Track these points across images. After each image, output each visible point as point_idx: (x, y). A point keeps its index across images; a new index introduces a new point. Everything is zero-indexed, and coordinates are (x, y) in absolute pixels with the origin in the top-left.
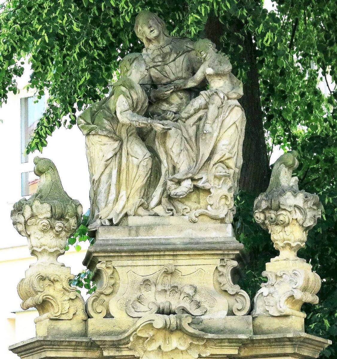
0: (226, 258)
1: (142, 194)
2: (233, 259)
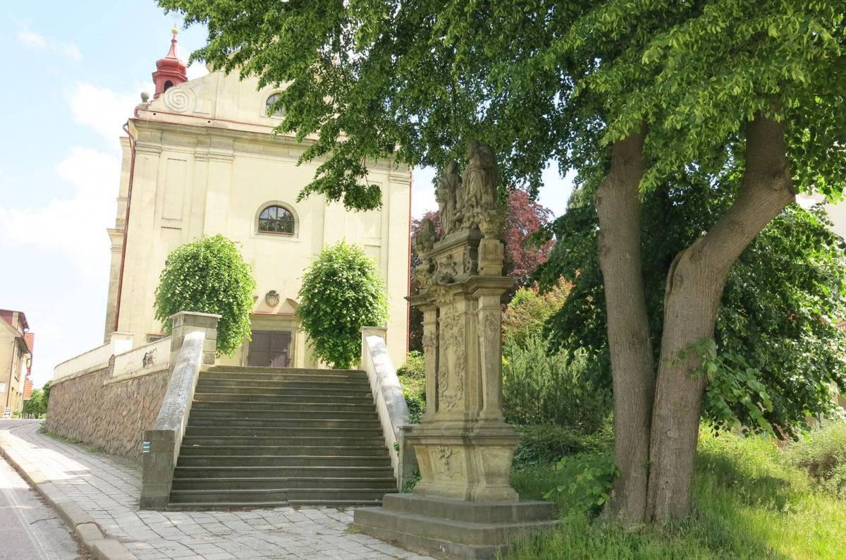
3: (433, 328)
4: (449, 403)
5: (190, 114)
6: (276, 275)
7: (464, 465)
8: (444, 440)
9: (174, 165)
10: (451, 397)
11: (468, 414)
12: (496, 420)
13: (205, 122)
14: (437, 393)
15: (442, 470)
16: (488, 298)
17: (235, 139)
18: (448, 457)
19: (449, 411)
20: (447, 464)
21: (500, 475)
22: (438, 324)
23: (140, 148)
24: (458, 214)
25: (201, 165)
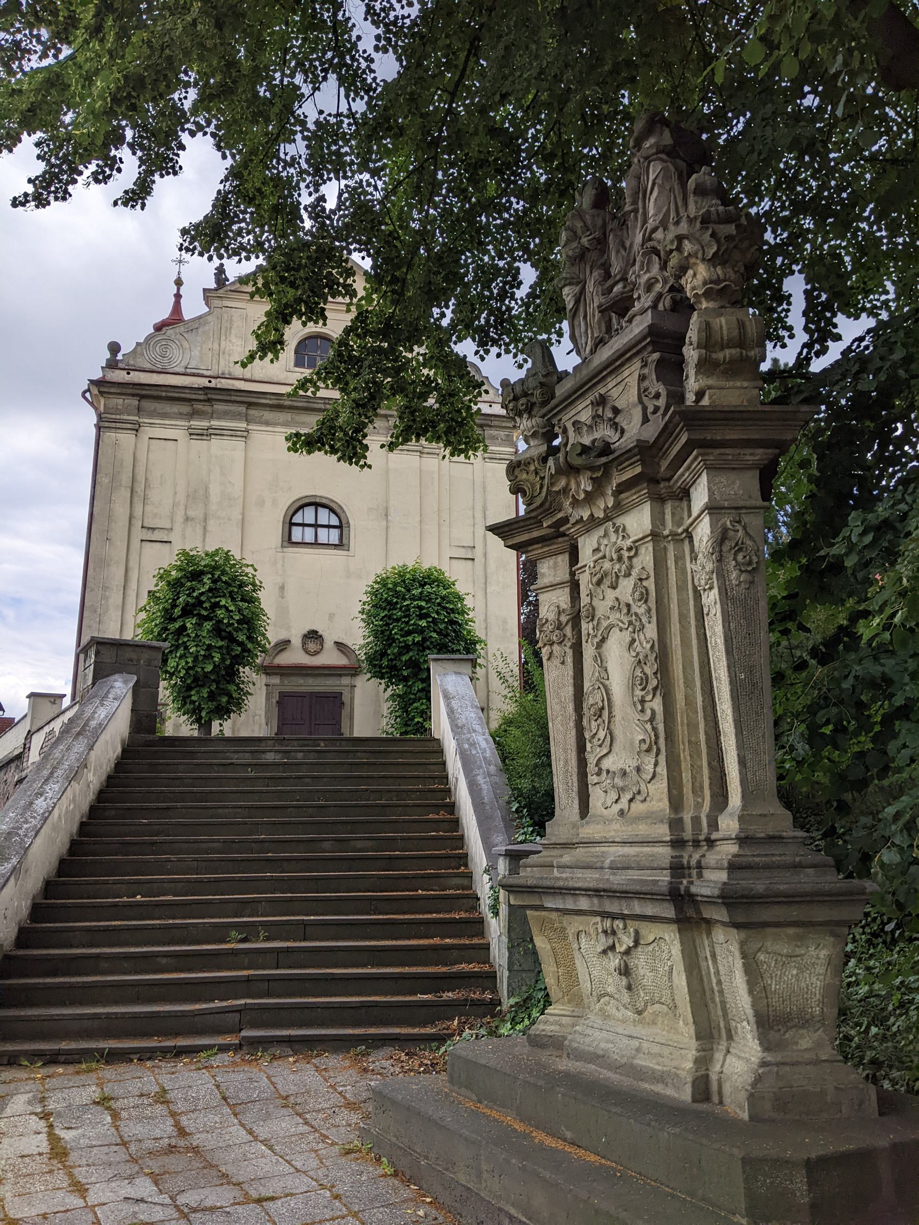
0: (645, 354)
1: (604, 329)
2: (654, 351)
3: (562, 598)
4: (621, 790)
5: (182, 370)
6: (315, 603)
7: (681, 981)
8: (613, 902)
9: (168, 449)
10: (624, 774)
11: (680, 821)
12: (774, 839)
13: (204, 382)
14: (582, 763)
15: (610, 989)
16: (723, 479)
17: (250, 405)
18: (628, 952)
19: (622, 813)
20: (625, 971)
21: (803, 1021)
22: (575, 586)
23: (107, 424)
24: (618, 288)
25: (199, 445)
